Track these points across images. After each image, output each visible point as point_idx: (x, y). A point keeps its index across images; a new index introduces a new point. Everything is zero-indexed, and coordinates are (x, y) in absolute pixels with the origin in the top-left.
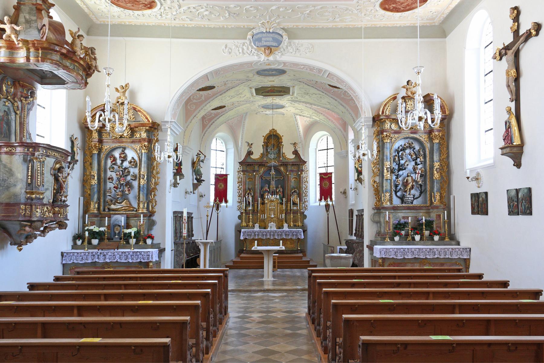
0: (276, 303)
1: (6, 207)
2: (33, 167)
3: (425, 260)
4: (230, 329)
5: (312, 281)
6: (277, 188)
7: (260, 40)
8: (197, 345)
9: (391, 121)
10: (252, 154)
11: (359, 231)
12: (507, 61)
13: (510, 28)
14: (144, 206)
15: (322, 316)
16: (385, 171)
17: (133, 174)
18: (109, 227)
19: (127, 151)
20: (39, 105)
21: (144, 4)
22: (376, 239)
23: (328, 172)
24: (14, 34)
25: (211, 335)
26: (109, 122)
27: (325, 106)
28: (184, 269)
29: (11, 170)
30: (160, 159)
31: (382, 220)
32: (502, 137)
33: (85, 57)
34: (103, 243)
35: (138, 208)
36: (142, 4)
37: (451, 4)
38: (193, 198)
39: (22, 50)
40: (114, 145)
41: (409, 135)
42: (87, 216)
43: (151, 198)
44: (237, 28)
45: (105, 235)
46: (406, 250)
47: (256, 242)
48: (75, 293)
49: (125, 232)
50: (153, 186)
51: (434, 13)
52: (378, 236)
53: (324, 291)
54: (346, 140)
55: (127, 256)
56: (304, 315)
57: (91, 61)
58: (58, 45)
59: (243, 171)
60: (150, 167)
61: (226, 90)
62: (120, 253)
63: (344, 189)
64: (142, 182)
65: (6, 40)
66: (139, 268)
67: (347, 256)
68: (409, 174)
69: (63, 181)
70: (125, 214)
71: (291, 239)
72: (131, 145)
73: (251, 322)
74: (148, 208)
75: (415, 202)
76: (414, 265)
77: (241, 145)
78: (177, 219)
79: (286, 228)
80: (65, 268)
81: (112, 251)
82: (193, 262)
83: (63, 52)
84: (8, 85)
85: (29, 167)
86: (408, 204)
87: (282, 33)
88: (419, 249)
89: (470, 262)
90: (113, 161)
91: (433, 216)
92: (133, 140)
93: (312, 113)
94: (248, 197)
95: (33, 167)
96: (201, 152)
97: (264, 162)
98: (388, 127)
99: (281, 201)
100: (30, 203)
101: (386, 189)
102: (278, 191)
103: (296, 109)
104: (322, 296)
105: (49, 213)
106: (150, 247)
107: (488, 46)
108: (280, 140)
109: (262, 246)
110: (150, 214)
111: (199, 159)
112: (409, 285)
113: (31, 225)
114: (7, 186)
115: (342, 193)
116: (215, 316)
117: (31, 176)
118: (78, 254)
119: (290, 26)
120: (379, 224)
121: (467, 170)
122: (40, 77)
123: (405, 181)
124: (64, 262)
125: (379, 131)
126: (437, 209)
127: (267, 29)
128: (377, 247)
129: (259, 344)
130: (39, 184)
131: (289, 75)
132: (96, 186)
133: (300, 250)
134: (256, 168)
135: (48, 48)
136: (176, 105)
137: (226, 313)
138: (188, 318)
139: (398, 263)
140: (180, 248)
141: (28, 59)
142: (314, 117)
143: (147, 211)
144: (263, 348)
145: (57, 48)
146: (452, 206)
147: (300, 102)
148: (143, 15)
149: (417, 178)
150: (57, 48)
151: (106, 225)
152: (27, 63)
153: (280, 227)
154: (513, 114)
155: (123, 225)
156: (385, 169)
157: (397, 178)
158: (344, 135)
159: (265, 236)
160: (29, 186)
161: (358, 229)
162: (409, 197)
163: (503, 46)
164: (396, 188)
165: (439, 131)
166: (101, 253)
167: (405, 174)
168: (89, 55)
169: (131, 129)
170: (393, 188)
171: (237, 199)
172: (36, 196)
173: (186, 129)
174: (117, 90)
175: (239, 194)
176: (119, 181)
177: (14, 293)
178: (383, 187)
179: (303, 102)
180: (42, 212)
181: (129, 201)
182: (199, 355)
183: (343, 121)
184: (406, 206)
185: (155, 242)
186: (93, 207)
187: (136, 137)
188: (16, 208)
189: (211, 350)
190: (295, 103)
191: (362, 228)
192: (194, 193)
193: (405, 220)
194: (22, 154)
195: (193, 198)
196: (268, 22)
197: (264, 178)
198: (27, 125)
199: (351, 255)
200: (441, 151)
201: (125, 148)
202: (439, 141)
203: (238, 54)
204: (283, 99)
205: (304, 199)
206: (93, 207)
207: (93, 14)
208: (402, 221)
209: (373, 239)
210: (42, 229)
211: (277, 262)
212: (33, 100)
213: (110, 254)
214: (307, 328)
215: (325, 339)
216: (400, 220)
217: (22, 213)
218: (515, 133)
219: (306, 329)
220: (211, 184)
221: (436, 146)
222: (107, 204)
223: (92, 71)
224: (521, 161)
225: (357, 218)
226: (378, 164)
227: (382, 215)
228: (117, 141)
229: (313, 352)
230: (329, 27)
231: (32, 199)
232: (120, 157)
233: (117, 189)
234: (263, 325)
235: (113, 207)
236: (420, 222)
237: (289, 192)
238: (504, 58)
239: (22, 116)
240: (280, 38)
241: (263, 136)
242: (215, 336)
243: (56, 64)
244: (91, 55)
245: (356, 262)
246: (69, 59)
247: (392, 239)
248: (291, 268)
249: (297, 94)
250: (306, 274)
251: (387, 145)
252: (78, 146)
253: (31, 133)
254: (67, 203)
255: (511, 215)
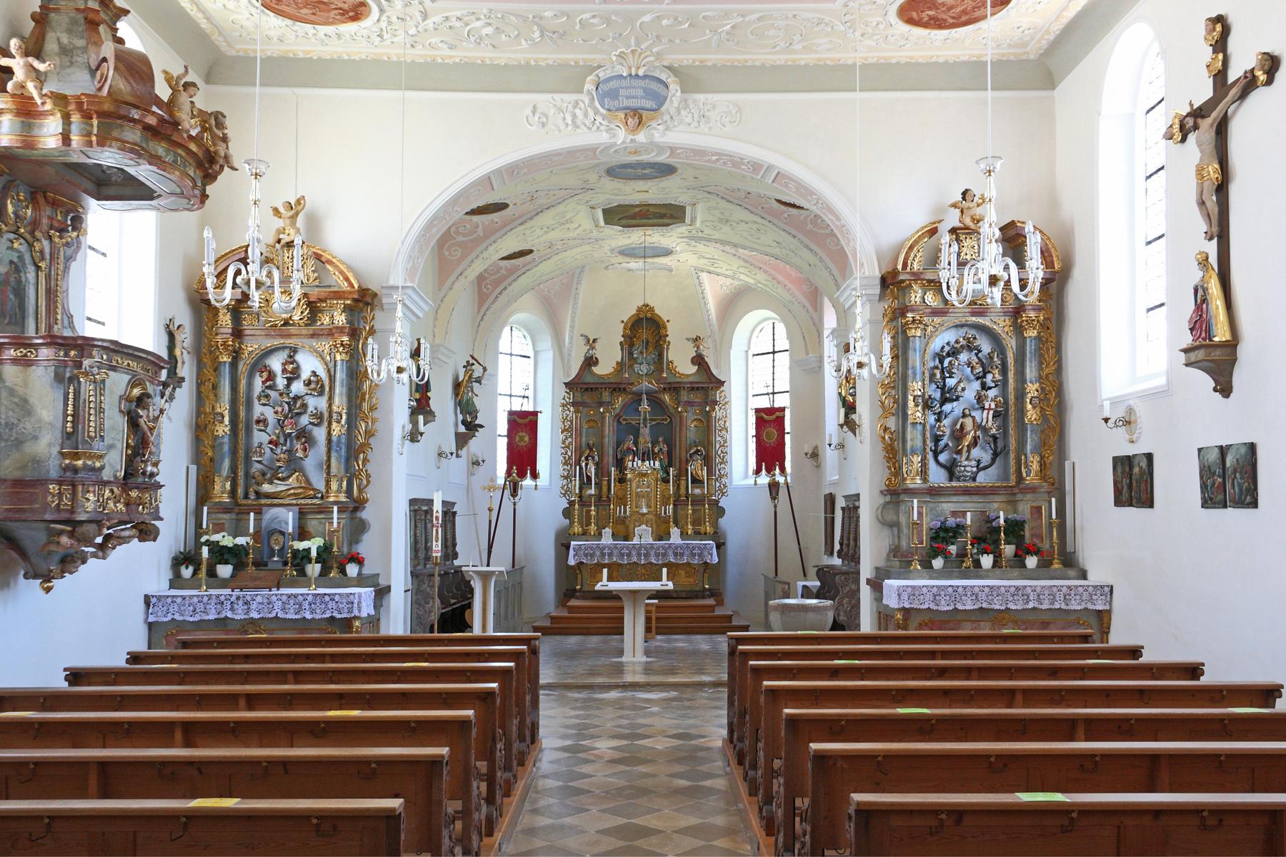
0: (652, 714)
1: (15, 488)
2: (77, 394)
3: (1004, 614)
4: (544, 777)
5: (737, 663)
6: (654, 443)
7: (613, 94)
8: (465, 814)
9: (924, 285)
10: (596, 362)
11: (848, 545)
12: (1199, 145)
13: (1205, 67)
14: (340, 486)
15: (760, 745)
16: (911, 404)
17: (314, 412)
18: (257, 536)
19: (299, 357)
20: (93, 249)
21: (340, 9)
22: (889, 564)
23: (776, 405)
24: (33, 81)
25: (498, 791)
26: (258, 288)
27: (768, 250)
28: (436, 634)
29: (26, 401)
30: (379, 375)
31: (903, 519)
32: (1187, 324)
33: (201, 135)
34: (242, 573)
35: (327, 492)
36: (336, 9)
37: (1065, 8)
38: (457, 466)
39: (51, 117)
40: (269, 343)
41: (967, 319)
42: (205, 509)
43: (357, 468)
44: (559, 65)
45: (247, 554)
46: (960, 590)
47: (605, 571)
48: (178, 691)
49: (295, 548)
50: (361, 440)
51: (1027, 32)
52: (894, 557)
53: (766, 686)
54: (818, 331)
55: (301, 605)
56: (719, 743)
57: (215, 144)
58: (137, 107)
59: (573, 404)
60: (354, 394)
61: (534, 213)
62: (284, 598)
63: (814, 445)
64: (337, 430)
65: (13, 96)
66: (330, 633)
67: (821, 604)
68: (967, 412)
69: (148, 426)
70: (297, 505)
71: (688, 564)
72: (310, 343)
73: (593, 761)
74: (349, 491)
75: (981, 478)
76: (979, 625)
77: (570, 343)
78: (418, 518)
79: (675, 537)
80: (153, 632)
81: (266, 592)
82: (456, 619)
83: (150, 122)
84: (19, 200)
85: (69, 393)
86: (964, 481)
87: (667, 79)
88: (991, 587)
89: (1110, 619)
90: (268, 379)
91: (1024, 510)
92: (314, 329)
93: (738, 268)
94: (587, 465)
95: (77, 394)
96: (476, 360)
97: (624, 382)
98: (918, 299)
99: (665, 475)
100: (71, 479)
101: (912, 447)
102: (656, 450)
103: (699, 258)
104: (762, 699)
105: (115, 503)
106: (354, 583)
107: (1153, 108)
108: (662, 331)
109: (619, 581)
110: (355, 506)
111: (471, 374)
112: (967, 672)
113: (74, 530)
114: (16, 439)
115: (808, 456)
116: (508, 746)
117: (72, 416)
118: (184, 599)
119: (685, 62)
120: (895, 529)
121: (1103, 401)
122: (94, 182)
123: (958, 427)
124: (151, 619)
125: (896, 309)
126: (1033, 492)
127: (630, 68)
128: (891, 584)
129: (613, 812)
130: (93, 434)
131: (682, 177)
132: (226, 440)
133: (709, 590)
134: (606, 396)
135: (114, 113)
136: (417, 247)
137: (534, 739)
138: (444, 751)
139: (941, 621)
140: (425, 586)
141: (66, 139)
142: (742, 277)
143: (347, 497)
144: (622, 821)
145: (136, 114)
146: (1068, 487)
147: (710, 240)
148: (339, 36)
149: (985, 420)
150: (136, 114)
151: (251, 530)
152: (64, 148)
153: (662, 535)
154: (1213, 269)
155: (290, 530)
156: (911, 398)
157: (938, 420)
158: (812, 319)
159: (625, 557)
160: (68, 439)
161: (845, 542)
162: (967, 466)
163: (1188, 109)
164: (936, 445)
165: (1037, 309)
166: (238, 598)
167: (958, 412)
168: (210, 129)
169: (310, 304)
170: (930, 444)
171: (560, 470)
172: (84, 464)
173: (440, 305)
174: (276, 211)
175: (565, 458)
176: (282, 427)
177: (33, 692)
178: (904, 441)
179: (717, 241)
180: (98, 501)
181: (304, 475)
182: (470, 839)
183: (811, 287)
184: (960, 486)
185: (366, 571)
186: (221, 489)
187: (322, 324)
188: (37, 491)
189: (499, 826)
190: (697, 244)
191: (857, 539)
192: (458, 456)
193: (958, 519)
194: (51, 363)
195: (457, 466)
196: (633, 52)
197: (624, 420)
198: (65, 294)
199: (829, 603)
200: (1041, 356)
201: (294, 350)
202: (1039, 333)
203: (562, 127)
204: (669, 234)
205: (719, 470)
206: (221, 489)
207: (220, 34)
208: (951, 522)
209: (881, 564)
210: (99, 540)
211: (654, 618)
212: (78, 236)
213: (259, 599)
214: (727, 774)
215: (768, 799)
216: (946, 520)
217: (53, 502)
218: (1218, 313)
219: (722, 776)
220: (499, 436)
221: (1031, 346)
222: (254, 481)
223: (217, 168)
224: (1231, 381)
225: (843, 514)
226: (894, 387)
227: (903, 507)
228: (277, 333)
229: (740, 831)
230: (778, 63)
231: (76, 470)
232: (283, 371)
233: (276, 445)
234: (622, 768)
235: (266, 488)
236: (994, 524)
237: (683, 454)
238: (1192, 138)
239: (53, 273)
240: (661, 89)
241: (623, 322)
242: (507, 794)
243: (132, 151)
244: (215, 129)
245: (841, 618)
246: (162, 139)
247: (927, 565)
248: (688, 633)
249: (702, 222)
250: (725, 648)
251: (914, 342)
252: (185, 345)
253: (72, 313)
254: (158, 478)
255: (1207, 508)
